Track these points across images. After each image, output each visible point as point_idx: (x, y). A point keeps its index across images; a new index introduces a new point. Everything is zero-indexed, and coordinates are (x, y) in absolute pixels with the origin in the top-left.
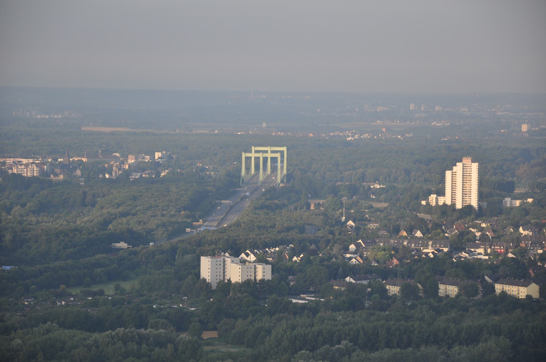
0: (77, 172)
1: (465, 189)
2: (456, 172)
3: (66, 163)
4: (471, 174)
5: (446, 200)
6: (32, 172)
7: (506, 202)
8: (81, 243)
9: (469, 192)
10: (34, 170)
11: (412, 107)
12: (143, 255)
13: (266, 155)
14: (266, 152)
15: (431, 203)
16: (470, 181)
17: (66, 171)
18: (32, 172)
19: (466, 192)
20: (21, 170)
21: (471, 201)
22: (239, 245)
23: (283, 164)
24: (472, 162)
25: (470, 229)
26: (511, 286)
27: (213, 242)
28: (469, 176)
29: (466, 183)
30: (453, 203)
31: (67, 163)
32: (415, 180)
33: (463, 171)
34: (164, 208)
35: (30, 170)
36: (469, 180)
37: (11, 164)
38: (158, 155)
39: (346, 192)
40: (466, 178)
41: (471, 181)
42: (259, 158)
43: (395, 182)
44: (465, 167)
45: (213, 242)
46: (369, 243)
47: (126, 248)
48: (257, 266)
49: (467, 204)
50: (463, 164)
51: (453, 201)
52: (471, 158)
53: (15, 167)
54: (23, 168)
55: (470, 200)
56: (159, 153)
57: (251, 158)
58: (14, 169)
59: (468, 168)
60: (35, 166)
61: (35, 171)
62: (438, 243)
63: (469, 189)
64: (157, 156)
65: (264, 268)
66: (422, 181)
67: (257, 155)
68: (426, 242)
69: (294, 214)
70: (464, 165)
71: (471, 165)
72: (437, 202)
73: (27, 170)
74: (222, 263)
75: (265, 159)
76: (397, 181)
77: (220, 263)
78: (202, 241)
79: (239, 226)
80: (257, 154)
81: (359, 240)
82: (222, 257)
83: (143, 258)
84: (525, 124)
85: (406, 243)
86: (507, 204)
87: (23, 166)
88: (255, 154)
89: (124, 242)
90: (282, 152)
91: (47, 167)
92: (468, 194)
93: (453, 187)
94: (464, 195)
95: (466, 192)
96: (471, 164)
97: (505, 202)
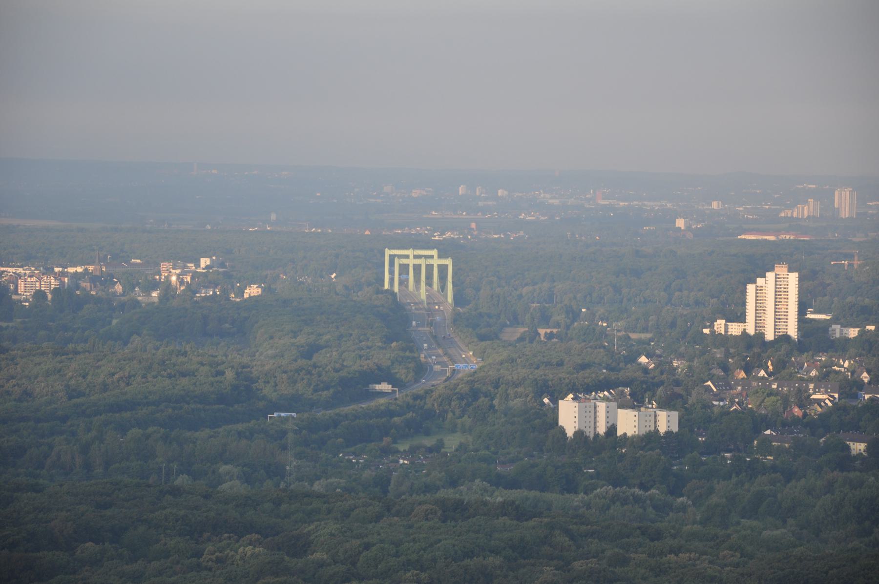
0: (116, 287)
1: (778, 312)
2: (761, 287)
4: (787, 288)
6: (48, 287)
7: (835, 330)
9: (785, 315)
11: (462, 190)
12: (434, 400)
13: (430, 261)
14: (407, 257)
16: (786, 300)
17: (99, 285)
18: (48, 287)
19: (780, 315)
21: (787, 329)
22: (551, 387)
23: (399, 278)
24: (788, 272)
25: (833, 368)
26: (858, 444)
27: (516, 383)
28: (785, 292)
29: (780, 302)
30: (757, 332)
31: (98, 273)
32: (629, 300)
34: (361, 338)
35: (45, 285)
36: (785, 298)
37: (11, 275)
38: (204, 262)
39: (563, 316)
40: (780, 295)
42: (420, 266)
44: (779, 278)
46: (722, 386)
47: (390, 391)
48: (658, 413)
49: (782, 334)
50: (776, 275)
51: (757, 328)
53: (22, 279)
54: (35, 280)
55: (786, 327)
56: (207, 259)
58: (19, 283)
59: (783, 280)
60: (52, 278)
62: (823, 386)
63: (784, 312)
64: (204, 263)
65: (669, 416)
66: (640, 302)
67: (418, 261)
71: (787, 276)
73: (41, 284)
74: (592, 410)
75: (429, 268)
76: (602, 301)
77: (590, 409)
79: (514, 362)
80: (417, 260)
81: (707, 381)
82: (591, 401)
83: (436, 405)
84: (681, 218)
85: (776, 386)
86: (835, 334)
87: (34, 277)
89: (386, 383)
90: (392, 258)
92: (783, 319)
94: (777, 320)
95: (780, 315)
96: (788, 275)
97: (832, 330)
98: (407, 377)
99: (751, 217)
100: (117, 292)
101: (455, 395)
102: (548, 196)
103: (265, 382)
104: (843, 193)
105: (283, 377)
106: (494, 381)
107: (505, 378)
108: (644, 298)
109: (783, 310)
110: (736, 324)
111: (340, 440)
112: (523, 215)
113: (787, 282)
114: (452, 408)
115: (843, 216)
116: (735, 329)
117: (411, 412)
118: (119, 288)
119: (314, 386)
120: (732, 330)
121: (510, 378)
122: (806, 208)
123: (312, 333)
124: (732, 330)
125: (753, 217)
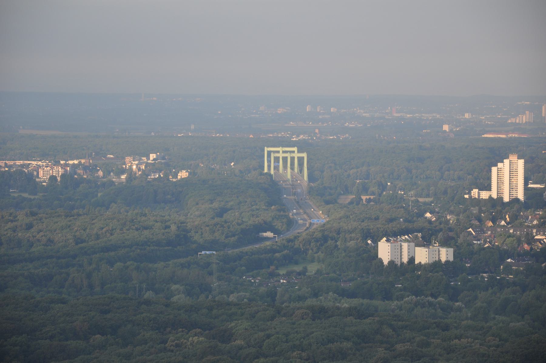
0: (99, 173)
1: (512, 184)
2: (501, 168)
3: (86, 165)
4: (517, 169)
5: (492, 194)
8: (237, 233)
9: (516, 186)
10: (59, 172)
11: (308, 108)
12: (300, 242)
13: (293, 155)
16: (516, 177)
17: (88, 172)
19: (513, 186)
20: (47, 172)
21: (517, 195)
22: (372, 233)
24: (518, 159)
27: (350, 231)
28: (516, 171)
29: (513, 178)
30: (498, 196)
31: (88, 164)
32: (417, 177)
33: (510, 167)
34: (252, 204)
35: (55, 172)
36: (516, 176)
37: (35, 166)
38: (152, 156)
39: (376, 188)
40: (513, 173)
41: (517, 176)
43: (397, 179)
44: (512, 163)
45: (350, 231)
47: (273, 237)
48: (441, 249)
49: (514, 198)
50: (510, 161)
51: (498, 194)
52: (517, 155)
53: (42, 169)
54: (49, 169)
57: (279, 157)
58: (40, 171)
59: (514, 164)
60: (60, 168)
61: (60, 172)
62: (542, 230)
63: (515, 184)
67: (285, 155)
68: (530, 230)
69: (375, 207)
70: (511, 162)
71: (517, 162)
72: (479, 196)
73: (53, 172)
75: (293, 159)
77: (398, 247)
78: (341, 230)
79: (348, 218)
81: (469, 228)
82: (399, 242)
83: (301, 245)
85: (512, 231)
87: (49, 168)
88: (283, 154)
89: (270, 232)
90: (269, 153)
91: (69, 168)
92: (515, 188)
93: (498, 182)
95: (513, 186)
96: (517, 161)
98: (282, 228)
99: (490, 123)
101: (313, 239)
102: (362, 111)
103: (195, 232)
105: (207, 229)
106: (337, 230)
107: (343, 228)
108: (426, 176)
109: (514, 183)
110: (485, 192)
111: (244, 268)
112: (347, 123)
114: (311, 247)
116: (485, 195)
117: (286, 250)
118: (101, 173)
119: (226, 234)
121: (346, 228)
122: (524, 117)
123: (222, 201)
124: (482, 196)
125: (491, 123)
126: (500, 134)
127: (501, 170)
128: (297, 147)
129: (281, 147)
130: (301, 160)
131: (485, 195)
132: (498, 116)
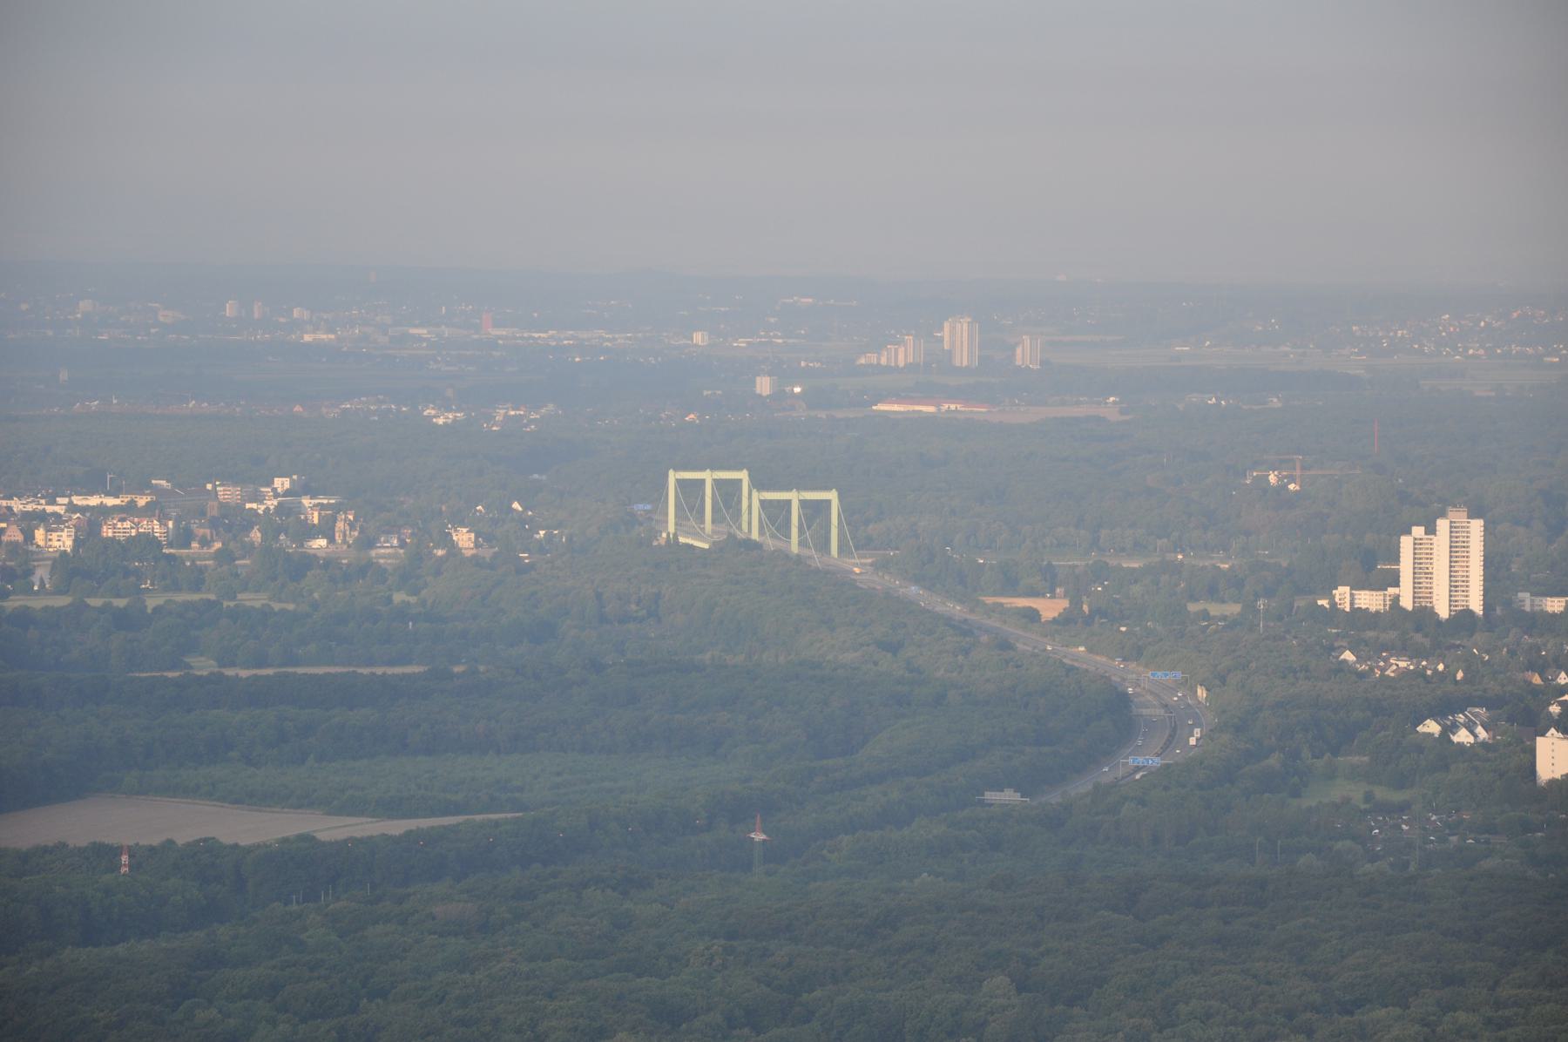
0: (252, 535)
1: (1454, 576)
2: (1421, 539)
7: (1524, 601)
15: (1340, 604)
16: (1465, 559)
24: (1468, 518)
40: (1457, 552)
44: (1455, 527)
50: (1451, 522)
53: (110, 525)
56: (284, 479)
58: (105, 530)
60: (155, 522)
63: (1463, 576)
86: (1524, 606)
87: (129, 522)
92: (1462, 586)
94: (1453, 589)
96: (1468, 522)
100: (254, 542)
104: (958, 325)
109: (1460, 573)
110: (1367, 592)
113: (1468, 532)
115: (958, 364)
116: (1370, 600)
120: (1360, 601)
122: (901, 350)
124: (1360, 601)
126: (918, 404)
127: (1421, 544)
128: (748, 470)
129: (708, 470)
130: (821, 508)
131: (1370, 600)
132: (774, 340)
